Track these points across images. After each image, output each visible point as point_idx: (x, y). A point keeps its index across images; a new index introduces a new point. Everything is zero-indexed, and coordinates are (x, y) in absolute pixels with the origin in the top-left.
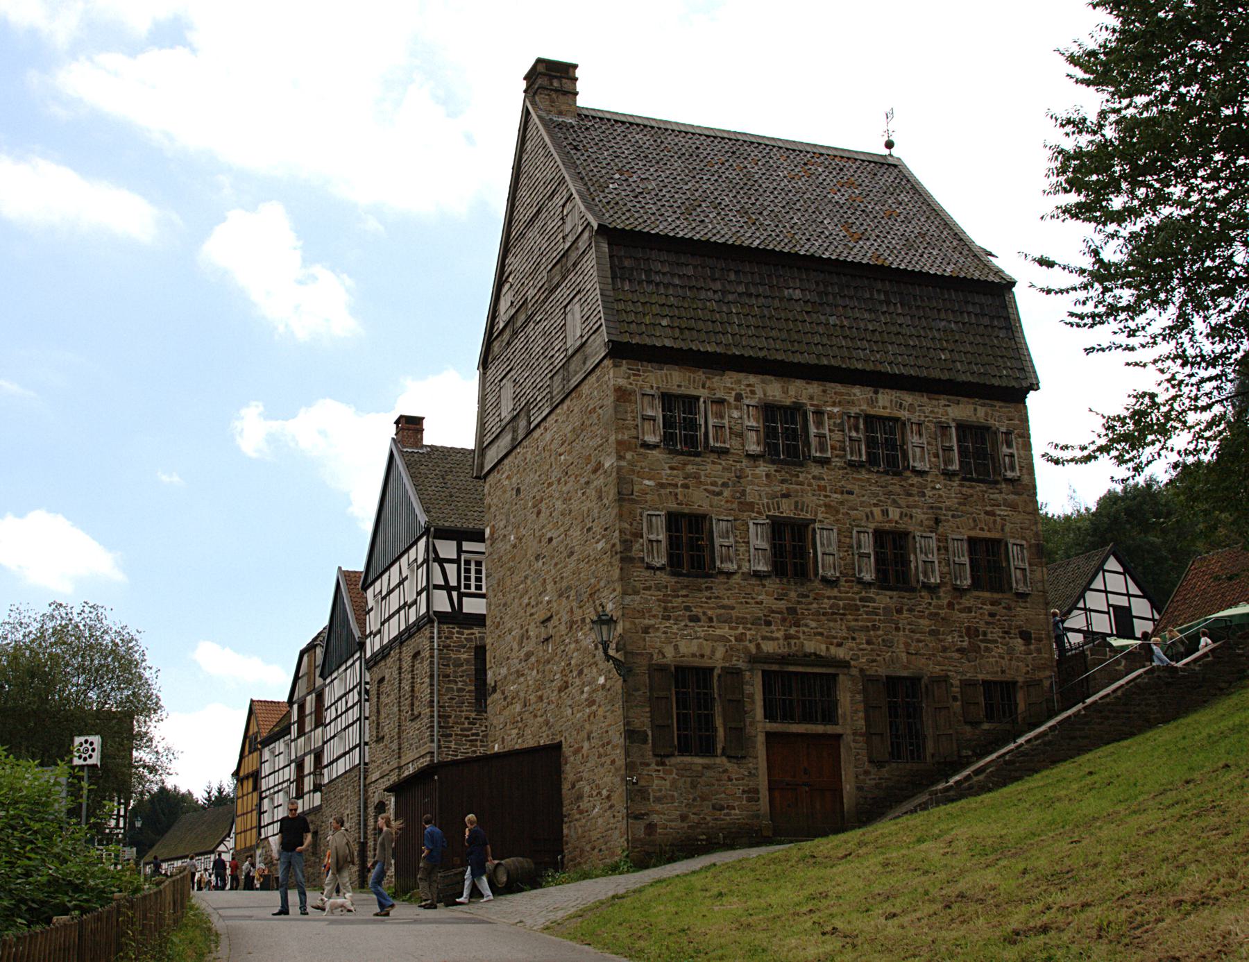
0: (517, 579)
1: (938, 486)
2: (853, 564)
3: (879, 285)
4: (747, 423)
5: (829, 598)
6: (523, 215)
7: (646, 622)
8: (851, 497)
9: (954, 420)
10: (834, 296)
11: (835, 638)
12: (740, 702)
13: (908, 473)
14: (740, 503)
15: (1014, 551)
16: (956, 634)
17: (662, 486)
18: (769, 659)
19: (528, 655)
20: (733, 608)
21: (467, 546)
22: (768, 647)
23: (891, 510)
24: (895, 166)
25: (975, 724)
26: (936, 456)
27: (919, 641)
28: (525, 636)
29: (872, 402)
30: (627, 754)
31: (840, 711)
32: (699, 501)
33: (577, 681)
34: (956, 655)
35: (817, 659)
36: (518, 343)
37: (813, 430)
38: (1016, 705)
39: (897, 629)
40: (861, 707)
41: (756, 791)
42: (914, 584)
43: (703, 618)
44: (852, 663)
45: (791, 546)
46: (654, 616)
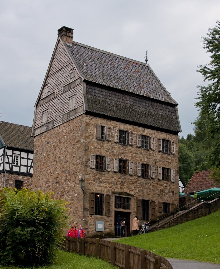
0: (45, 165)
1: (157, 154)
2: (137, 172)
3: (147, 102)
4: (115, 134)
5: (131, 179)
6: (54, 69)
7: (90, 182)
8: (137, 155)
9: (161, 138)
10: (137, 103)
11: (131, 189)
12: (109, 203)
13: (150, 150)
14: (112, 154)
15: (172, 171)
16: (158, 190)
17: (95, 148)
18: (116, 193)
19: (49, 186)
20: (109, 180)
21: (15, 152)
22: (117, 190)
23: (146, 159)
24: (148, 67)
25: (160, 212)
26: (157, 146)
27: (150, 191)
28: (48, 181)
29: (144, 132)
30: (84, 213)
31: (131, 207)
32: (103, 153)
33: (67, 194)
34: (157, 196)
35: (126, 194)
36: (51, 103)
37: (130, 137)
38: (169, 209)
39: (145, 188)
40: (136, 206)
41: (112, 225)
42: (149, 177)
43: (102, 182)
44: (135, 195)
45: (123, 166)
46: (92, 180)
